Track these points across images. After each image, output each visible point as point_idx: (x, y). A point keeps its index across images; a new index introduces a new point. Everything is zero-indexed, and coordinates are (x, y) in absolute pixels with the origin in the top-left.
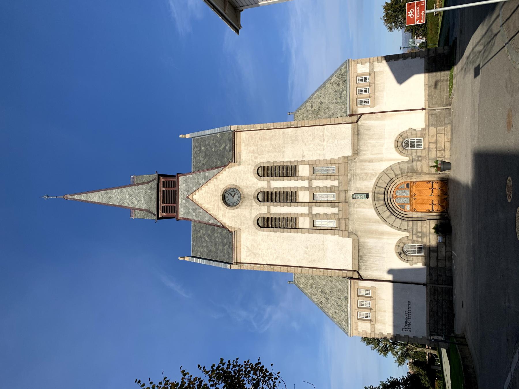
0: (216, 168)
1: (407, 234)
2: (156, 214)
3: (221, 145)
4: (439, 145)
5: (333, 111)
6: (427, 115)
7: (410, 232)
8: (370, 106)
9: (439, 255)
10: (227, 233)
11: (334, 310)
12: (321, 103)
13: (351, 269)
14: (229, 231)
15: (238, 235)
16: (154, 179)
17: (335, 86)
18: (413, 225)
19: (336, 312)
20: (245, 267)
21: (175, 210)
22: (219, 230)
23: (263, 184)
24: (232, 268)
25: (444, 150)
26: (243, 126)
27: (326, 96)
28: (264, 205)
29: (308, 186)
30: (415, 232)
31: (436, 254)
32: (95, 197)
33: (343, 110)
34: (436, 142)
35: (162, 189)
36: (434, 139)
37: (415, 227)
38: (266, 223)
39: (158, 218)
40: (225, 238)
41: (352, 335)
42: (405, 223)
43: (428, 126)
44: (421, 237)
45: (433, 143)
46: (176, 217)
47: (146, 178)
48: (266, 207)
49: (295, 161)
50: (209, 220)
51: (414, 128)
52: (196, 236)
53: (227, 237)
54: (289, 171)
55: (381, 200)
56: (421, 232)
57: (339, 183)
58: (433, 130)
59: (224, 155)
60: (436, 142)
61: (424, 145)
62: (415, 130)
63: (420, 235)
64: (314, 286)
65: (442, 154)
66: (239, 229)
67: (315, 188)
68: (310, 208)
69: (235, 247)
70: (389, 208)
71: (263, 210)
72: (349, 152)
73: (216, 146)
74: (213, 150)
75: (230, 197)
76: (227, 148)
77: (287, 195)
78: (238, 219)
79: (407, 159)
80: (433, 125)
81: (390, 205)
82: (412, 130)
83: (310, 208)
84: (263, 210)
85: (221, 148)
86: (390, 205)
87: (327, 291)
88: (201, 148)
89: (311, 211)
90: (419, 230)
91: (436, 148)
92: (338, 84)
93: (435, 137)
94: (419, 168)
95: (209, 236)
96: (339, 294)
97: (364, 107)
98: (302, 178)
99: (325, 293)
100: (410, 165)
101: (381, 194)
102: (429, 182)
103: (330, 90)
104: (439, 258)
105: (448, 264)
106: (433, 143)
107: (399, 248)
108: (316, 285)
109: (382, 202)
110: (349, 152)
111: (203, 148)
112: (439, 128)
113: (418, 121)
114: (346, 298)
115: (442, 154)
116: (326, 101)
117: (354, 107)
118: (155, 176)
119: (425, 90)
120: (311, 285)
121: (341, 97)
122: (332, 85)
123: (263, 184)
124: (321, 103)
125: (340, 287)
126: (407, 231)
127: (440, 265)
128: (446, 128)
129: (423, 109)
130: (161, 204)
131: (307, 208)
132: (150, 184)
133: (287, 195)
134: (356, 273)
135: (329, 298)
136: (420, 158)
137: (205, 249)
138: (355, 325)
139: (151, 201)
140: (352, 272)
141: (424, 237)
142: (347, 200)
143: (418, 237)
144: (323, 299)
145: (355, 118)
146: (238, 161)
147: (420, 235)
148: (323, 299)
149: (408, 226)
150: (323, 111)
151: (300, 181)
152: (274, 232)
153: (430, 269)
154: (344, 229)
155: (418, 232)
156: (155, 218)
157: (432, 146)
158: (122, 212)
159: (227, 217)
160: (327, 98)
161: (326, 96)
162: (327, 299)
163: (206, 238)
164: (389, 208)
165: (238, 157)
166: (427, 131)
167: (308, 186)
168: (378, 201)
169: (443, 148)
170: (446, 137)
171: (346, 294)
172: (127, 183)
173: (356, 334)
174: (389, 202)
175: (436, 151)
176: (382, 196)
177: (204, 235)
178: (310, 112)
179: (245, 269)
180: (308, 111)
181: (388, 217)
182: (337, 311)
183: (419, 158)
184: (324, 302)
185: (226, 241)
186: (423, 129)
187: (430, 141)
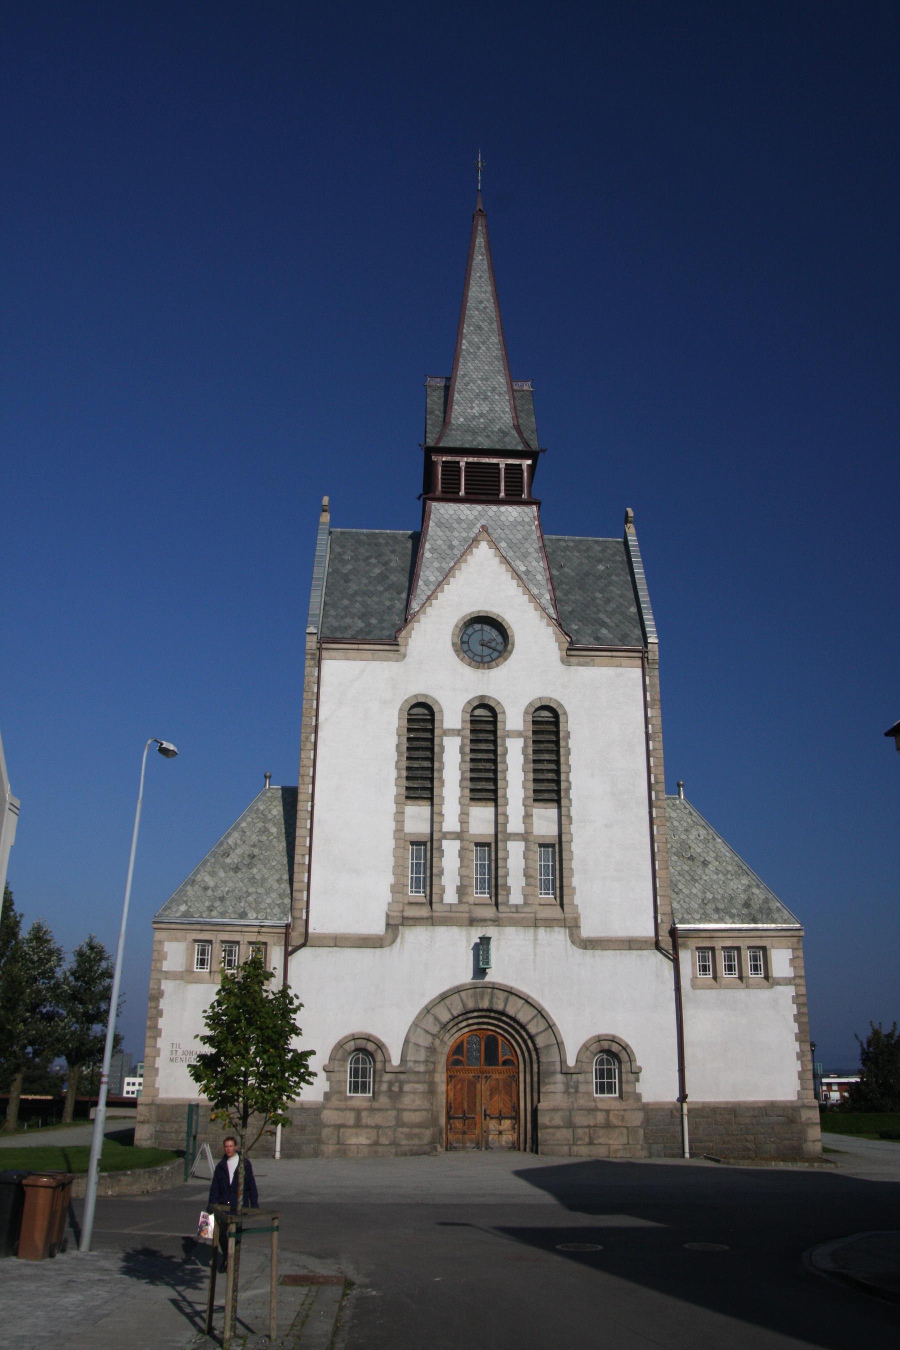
0: (555, 602)
1: (396, 1061)
2: (441, 445)
3: (611, 614)
4: (601, 1132)
5: (686, 891)
6: (671, 1106)
7: (400, 1065)
8: (695, 978)
9: (349, 1130)
10: (394, 625)
11: (211, 884)
12: (705, 863)
13: (311, 930)
14: (399, 630)
15: (391, 654)
16: (526, 443)
17: (743, 896)
18: (419, 1072)
19: (206, 889)
20: (310, 671)
21: (451, 496)
22: (399, 606)
23: (514, 719)
24: (308, 638)
25: (591, 1143)
26: (657, 673)
27: (720, 876)
28: (463, 721)
29: (508, 831)
30: (403, 1077)
31: (351, 1122)
32: (480, 291)
33: (686, 916)
34: (608, 1126)
35: (502, 463)
36: (614, 1121)
37: (413, 1077)
38: (421, 722)
39: (429, 451)
40: (381, 621)
41: (156, 926)
42: (422, 1055)
43: (647, 1109)
44: (390, 1089)
45: (607, 1119)
46: (428, 493)
47: (530, 422)
48: (459, 726)
49: (570, 800)
50: (427, 583)
51: (641, 1075)
52: (381, 541)
53: (383, 631)
54: (549, 786)
55: (476, 1002)
56: (401, 1089)
57: (516, 906)
58: (637, 1119)
59: (583, 633)
60: (608, 1126)
61: (601, 1100)
62: (638, 1080)
63: (395, 1088)
64: (264, 838)
65: (580, 1139)
66: (404, 656)
67: (525, 896)
68: (459, 836)
69: (361, 647)
70: (456, 1021)
71: (452, 717)
72: (586, 932)
73: (608, 601)
74: (599, 595)
75: (484, 638)
76: (604, 631)
77: (480, 770)
78: (431, 665)
79: (571, 1062)
80: (647, 1121)
81: (464, 1023)
82: (636, 1073)
83: (459, 836)
84: (452, 717)
85: (602, 616)
86: (464, 1023)
87: (255, 871)
88: (600, 561)
89: (448, 836)
90: (407, 1088)
91: (595, 1126)
92: (747, 905)
93: (620, 1124)
94: (551, 1088)
95: (382, 578)
96: (250, 898)
97: (694, 965)
98: (528, 816)
99: (250, 866)
100: (558, 1068)
101: (491, 1001)
102: (516, 1108)
103: (734, 884)
104: (342, 1130)
105: (329, 1148)
106: (607, 1119)
107: (364, 1042)
108: (267, 843)
109: (471, 1005)
110: (586, 932)
111: (601, 567)
112: (641, 1131)
113: (656, 1086)
114: (243, 915)
115: (580, 1139)
116: (709, 874)
117: (693, 943)
118: (535, 445)
119: (727, 1103)
120: (265, 831)
121: (717, 910)
122: (745, 891)
123: (514, 719)
124: (705, 863)
125: (269, 901)
126: (403, 1060)
127: (326, 1132)
128: (639, 1147)
129: (683, 1097)
130: (463, 461)
131: (457, 828)
132: (514, 432)
133: (480, 770)
134: (302, 941)
135: (240, 875)
136: (572, 1090)
137: (350, 567)
138: (179, 934)
139: (474, 432)
140: (304, 930)
141: (390, 1097)
142: (475, 923)
143: (391, 1084)
144: (233, 859)
145: (666, 941)
146: (573, 659)
147: (395, 1088)
148: (233, 859)
149: (416, 1062)
150: (687, 868)
151: (521, 811)
152: (398, 746)
153: (317, 1109)
154: (406, 914)
155: (402, 1084)
156: (430, 442)
157: (600, 1117)
158: (442, 359)
159: (433, 631)
160: (715, 877)
161: (720, 876)
162: (236, 869)
163: (377, 571)
164: (456, 1021)
165: (581, 659)
166: (635, 1106)
167: (508, 831)
168: (474, 996)
169: (596, 1142)
170: (620, 1147)
171: (252, 914)
172: (517, 362)
173: (159, 935)
174: (471, 1021)
175: (589, 1126)
176: (485, 1004)
177: (386, 564)
178: (684, 837)
179: (307, 670)
180: (687, 830)
181: (436, 1019)
182: (210, 892)
183: (572, 1089)
184: (228, 860)
185: (374, 621)
186: (638, 1097)
187: (611, 1113)
